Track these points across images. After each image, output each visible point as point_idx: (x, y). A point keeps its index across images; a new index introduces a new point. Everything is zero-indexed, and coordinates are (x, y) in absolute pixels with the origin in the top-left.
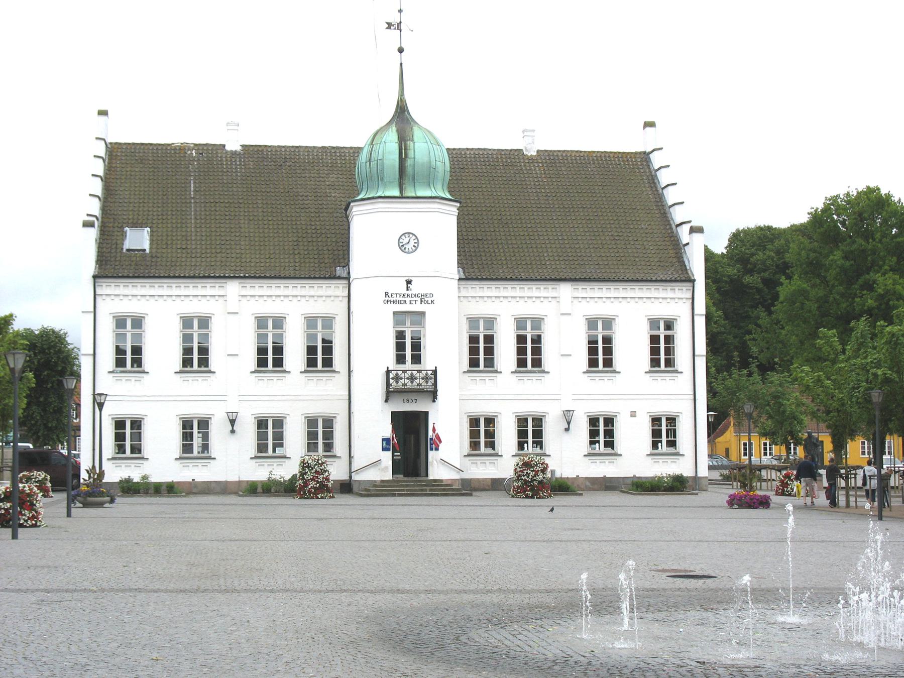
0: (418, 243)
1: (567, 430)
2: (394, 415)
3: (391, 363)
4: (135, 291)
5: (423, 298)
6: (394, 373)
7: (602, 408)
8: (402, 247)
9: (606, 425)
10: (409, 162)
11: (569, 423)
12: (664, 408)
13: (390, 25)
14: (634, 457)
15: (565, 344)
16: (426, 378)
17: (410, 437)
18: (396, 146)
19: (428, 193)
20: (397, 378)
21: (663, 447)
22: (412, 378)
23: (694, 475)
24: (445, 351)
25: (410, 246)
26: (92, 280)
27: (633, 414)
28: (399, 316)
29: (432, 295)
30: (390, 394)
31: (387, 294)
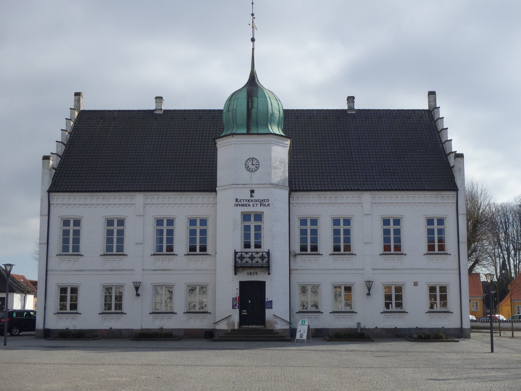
1: (369, 294)
3: (239, 248)
4: (77, 201)
5: (262, 202)
6: (240, 254)
8: (248, 169)
10: (254, 111)
11: (369, 290)
12: (438, 280)
14: (417, 313)
15: (367, 235)
16: (262, 258)
17: (252, 298)
18: (245, 101)
20: (242, 258)
22: (252, 258)
23: (460, 327)
24: (277, 239)
26: (47, 193)
27: (416, 284)
28: (246, 217)
29: (268, 200)
30: (237, 269)
31: (237, 200)
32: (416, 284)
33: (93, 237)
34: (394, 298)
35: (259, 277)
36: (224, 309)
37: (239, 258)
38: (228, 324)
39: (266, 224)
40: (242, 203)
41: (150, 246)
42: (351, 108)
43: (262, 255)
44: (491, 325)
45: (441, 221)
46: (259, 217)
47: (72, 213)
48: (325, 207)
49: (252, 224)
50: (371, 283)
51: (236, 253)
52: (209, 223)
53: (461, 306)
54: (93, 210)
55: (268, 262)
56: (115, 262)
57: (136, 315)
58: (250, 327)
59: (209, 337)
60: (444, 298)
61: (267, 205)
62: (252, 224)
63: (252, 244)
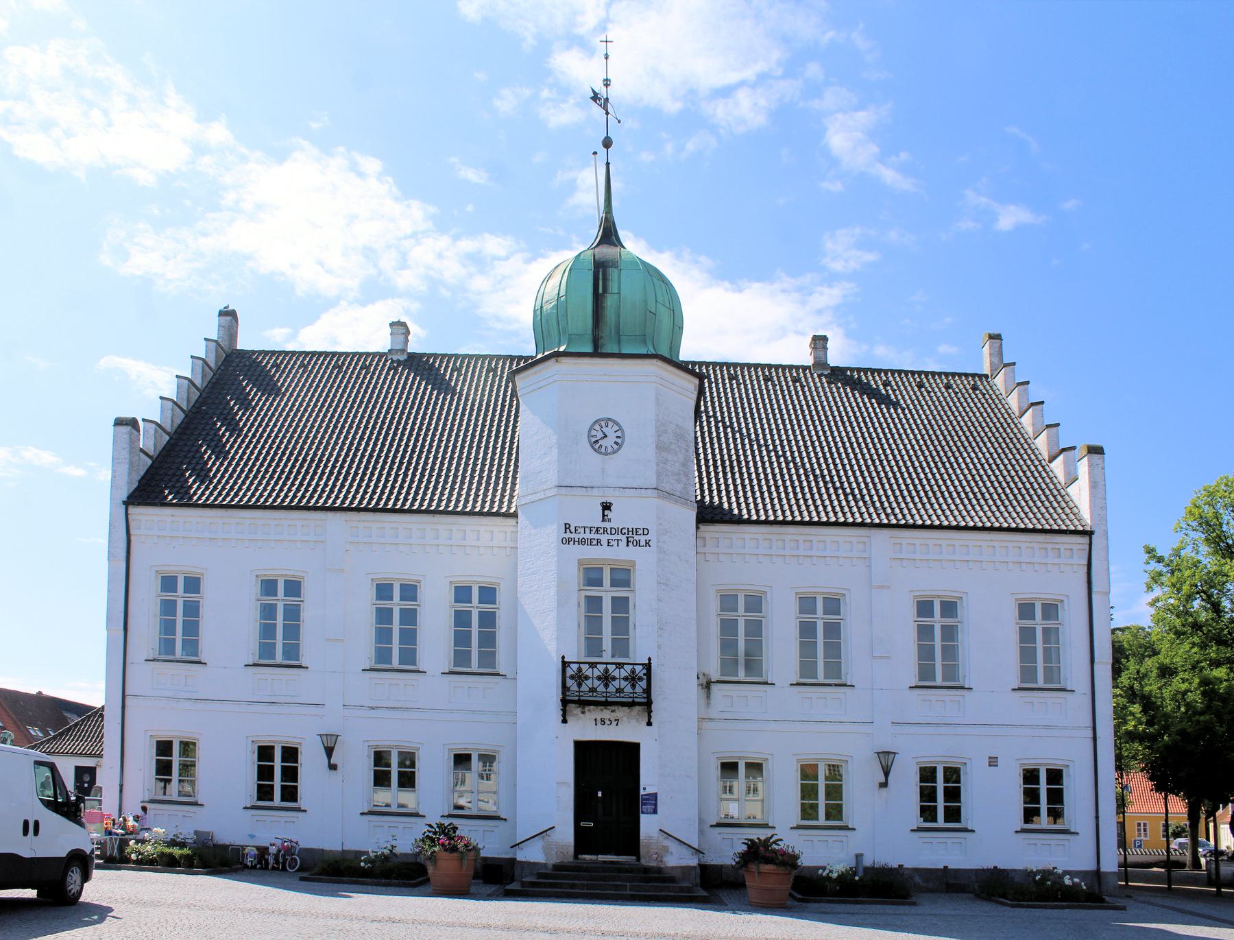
0: (621, 429)
1: (884, 785)
2: (583, 750)
5: (632, 536)
6: (575, 667)
7: (938, 753)
8: (594, 444)
10: (610, 301)
11: (887, 774)
12: (1043, 757)
13: (595, 97)
15: (881, 639)
16: (633, 679)
17: (608, 781)
20: (580, 678)
21: (1044, 821)
22: (606, 678)
23: (1093, 867)
27: (993, 762)
28: (592, 576)
29: (646, 531)
31: (567, 527)
32: (993, 762)
33: (229, 623)
34: (941, 796)
35: (624, 729)
36: (541, 807)
37: (572, 677)
38: (546, 850)
39: (643, 596)
40: (581, 536)
41: (364, 647)
42: (820, 364)
43: (633, 671)
44: (1169, 872)
45: (1051, 610)
46: (622, 577)
47: (181, 562)
48: (778, 567)
49: (607, 594)
50: (891, 756)
51: (565, 664)
52: (501, 596)
53: (1097, 817)
54: (223, 548)
55: (648, 691)
56: (279, 681)
57: (334, 811)
58: (601, 858)
59: (499, 878)
60: (1056, 797)
61: (643, 543)
62: (607, 594)
63: (607, 644)
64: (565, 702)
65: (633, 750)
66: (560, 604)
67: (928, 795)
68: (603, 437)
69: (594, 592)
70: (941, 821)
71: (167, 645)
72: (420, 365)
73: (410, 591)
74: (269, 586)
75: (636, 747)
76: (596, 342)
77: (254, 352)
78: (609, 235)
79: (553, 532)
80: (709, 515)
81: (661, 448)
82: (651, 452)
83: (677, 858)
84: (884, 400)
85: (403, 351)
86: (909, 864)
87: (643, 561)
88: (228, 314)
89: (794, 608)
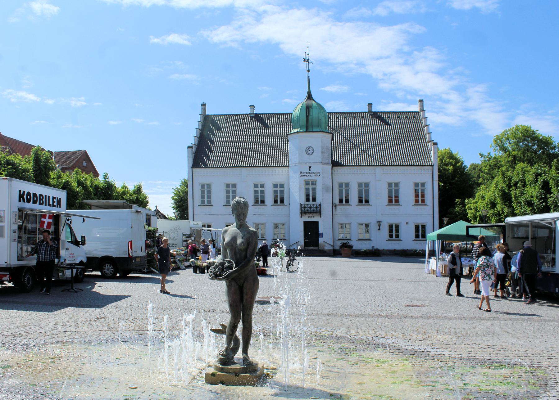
2: (305, 223)
5: (316, 174)
7: (394, 221)
8: (307, 152)
9: (396, 228)
10: (310, 117)
13: (305, 60)
15: (379, 196)
16: (317, 207)
17: (311, 230)
19: (318, 130)
20: (305, 208)
22: (310, 207)
23: (334, 168)
25: (311, 149)
27: (407, 223)
28: (307, 183)
29: (319, 173)
30: (302, 213)
31: (301, 172)
32: (407, 223)
35: (315, 219)
45: (423, 185)
46: (314, 183)
47: (206, 181)
48: (352, 177)
51: (301, 205)
52: (285, 186)
55: (320, 210)
64: (301, 213)
65: (317, 223)
66: (300, 190)
67: (391, 231)
68: (309, 151)
69: (308, 187)
70: (394, 238)
71: (203, 202)
72: (257, 117)
73: (263, 186)
74: (228, 186)
75: (318, 222)
76: (307, 128)
77: (212, 115)
78: (310, 97)
79: (298, 175)
80: (335, 164)
81: (323, 153)
82: (320, 154)
83: (328, 248)
84: (387, 124)
85: (253, 113)
86: (385, 249)
87: (319, 180)
88: (204, 105)
89: (357, 186)
